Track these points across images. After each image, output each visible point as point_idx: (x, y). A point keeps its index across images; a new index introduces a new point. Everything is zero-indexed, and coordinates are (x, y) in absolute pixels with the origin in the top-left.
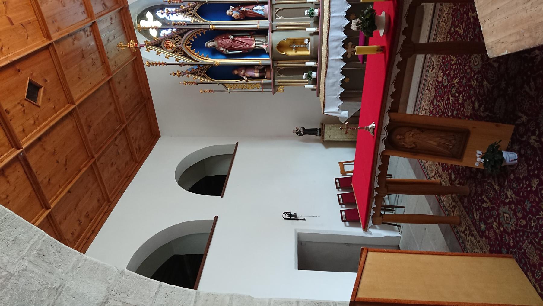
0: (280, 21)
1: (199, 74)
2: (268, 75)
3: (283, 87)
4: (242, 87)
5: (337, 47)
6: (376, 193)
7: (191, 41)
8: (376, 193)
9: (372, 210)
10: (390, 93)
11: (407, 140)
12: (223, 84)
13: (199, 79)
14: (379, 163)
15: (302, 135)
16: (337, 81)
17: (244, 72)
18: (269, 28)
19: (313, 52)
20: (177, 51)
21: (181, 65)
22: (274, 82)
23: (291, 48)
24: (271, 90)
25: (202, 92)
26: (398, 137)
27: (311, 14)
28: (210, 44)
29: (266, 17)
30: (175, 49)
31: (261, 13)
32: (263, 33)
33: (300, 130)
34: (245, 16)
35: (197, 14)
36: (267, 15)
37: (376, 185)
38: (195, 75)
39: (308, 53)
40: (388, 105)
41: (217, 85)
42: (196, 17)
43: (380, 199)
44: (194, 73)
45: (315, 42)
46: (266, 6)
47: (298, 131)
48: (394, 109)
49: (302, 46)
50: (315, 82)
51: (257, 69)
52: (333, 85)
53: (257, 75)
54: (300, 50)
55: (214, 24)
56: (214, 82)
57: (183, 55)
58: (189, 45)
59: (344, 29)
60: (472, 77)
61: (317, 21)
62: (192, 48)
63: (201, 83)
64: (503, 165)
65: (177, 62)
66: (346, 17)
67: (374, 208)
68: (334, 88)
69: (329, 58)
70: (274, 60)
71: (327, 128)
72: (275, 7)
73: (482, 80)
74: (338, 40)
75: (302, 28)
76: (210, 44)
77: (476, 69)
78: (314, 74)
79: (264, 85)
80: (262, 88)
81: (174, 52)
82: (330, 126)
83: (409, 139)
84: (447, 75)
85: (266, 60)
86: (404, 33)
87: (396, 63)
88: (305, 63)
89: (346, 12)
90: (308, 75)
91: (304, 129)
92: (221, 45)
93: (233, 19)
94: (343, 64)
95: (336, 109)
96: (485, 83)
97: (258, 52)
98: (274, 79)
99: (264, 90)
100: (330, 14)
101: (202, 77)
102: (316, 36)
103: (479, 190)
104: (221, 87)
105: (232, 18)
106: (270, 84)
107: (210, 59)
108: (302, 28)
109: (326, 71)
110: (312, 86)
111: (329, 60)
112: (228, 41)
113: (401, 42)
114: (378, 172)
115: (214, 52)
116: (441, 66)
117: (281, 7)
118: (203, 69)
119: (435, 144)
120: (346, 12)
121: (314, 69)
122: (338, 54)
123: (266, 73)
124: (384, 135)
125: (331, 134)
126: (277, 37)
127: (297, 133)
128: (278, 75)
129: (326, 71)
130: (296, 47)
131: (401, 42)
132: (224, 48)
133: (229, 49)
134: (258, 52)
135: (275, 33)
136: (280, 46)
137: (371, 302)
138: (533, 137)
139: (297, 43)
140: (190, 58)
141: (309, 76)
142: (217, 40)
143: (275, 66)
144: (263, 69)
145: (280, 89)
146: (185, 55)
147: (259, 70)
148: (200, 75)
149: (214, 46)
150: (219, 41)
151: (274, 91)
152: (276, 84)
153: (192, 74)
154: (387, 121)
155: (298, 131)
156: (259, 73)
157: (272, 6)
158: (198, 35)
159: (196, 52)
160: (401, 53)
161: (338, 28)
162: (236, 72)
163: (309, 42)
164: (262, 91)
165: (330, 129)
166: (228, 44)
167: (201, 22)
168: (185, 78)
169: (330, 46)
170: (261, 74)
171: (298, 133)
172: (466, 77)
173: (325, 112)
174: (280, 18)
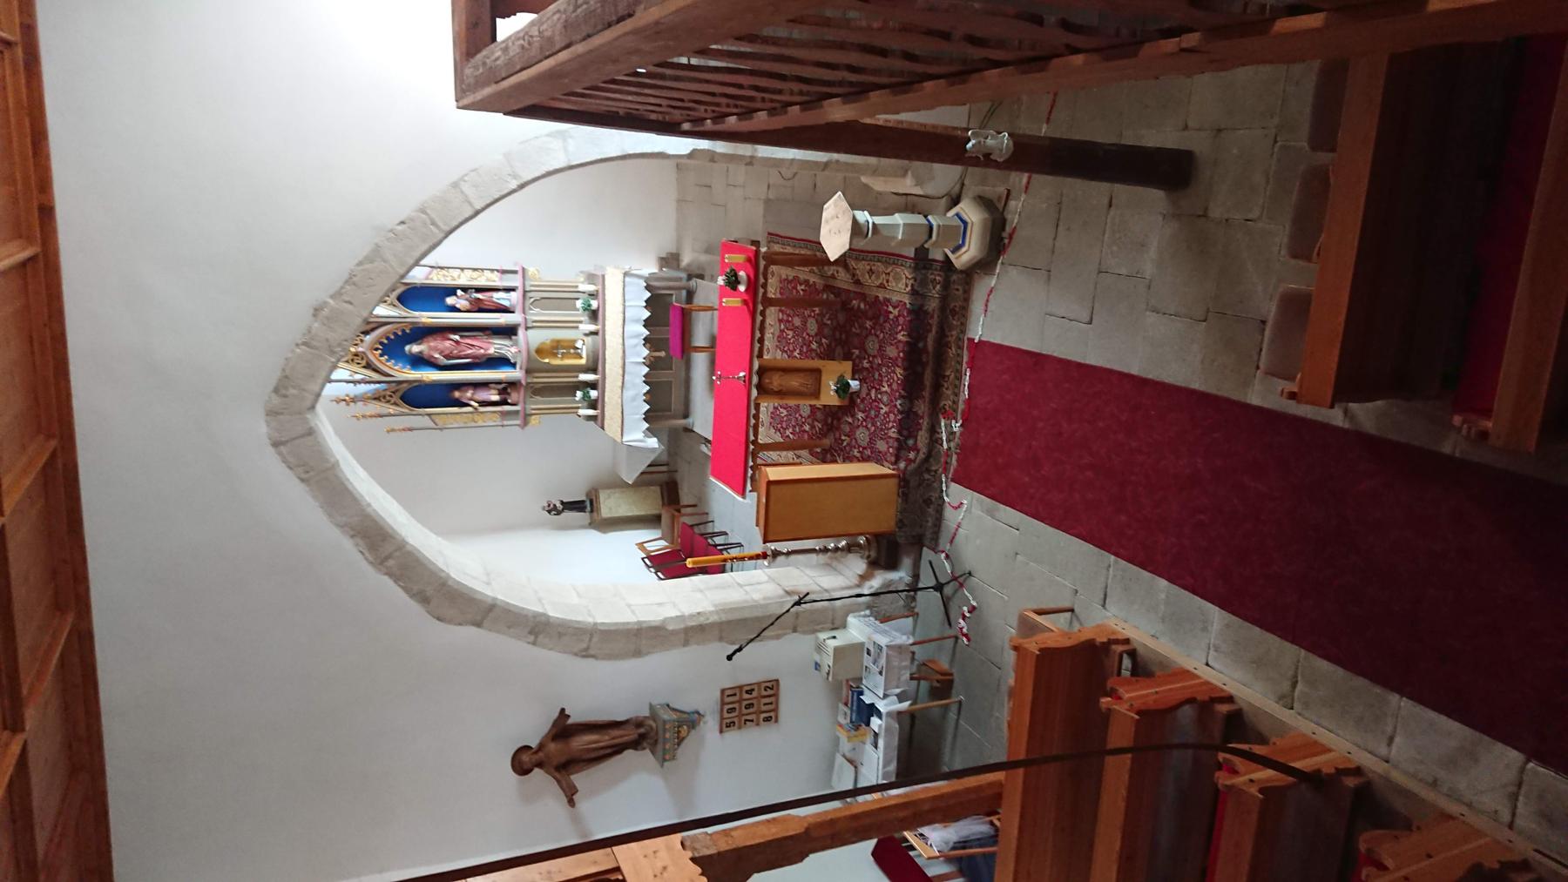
0: (536, 314)
1: (388, 398)
2: (513, 397)
3: (538, 416)
4: (466, 420)
5: (636, 346)
6: (752, 447)
7: (381, 343)
8: (752, 447)
9: (750, 470)
10: (757, 338)
11: (775, 384)
12: (429, 415)
13: (392, 409)
14: (753, 411)
15: (559, 513)
16: (637, 395)
17: (473, 394)
18: (519, 325)
19: (591, 360)
20: (352, 360)
21: (355, 382)
22: (525, 409)
23: (555, 355)
24: (518, 422)
25: (388, 432)
26: (767, 381)
27: (587, 308)
28: (415, 348)
29: (512, 310)
30: (350, 357)
31: (506, 303)
32: (509, 332)
33: (555, 505)
34: (479, 307)
35: (397, 303)
36: (514, 307)
37: (752, 438)
38: (380, 400)
39: (583, 361)
40: (756, 352)
41: (420, 418)
42: (394, 306)
43: (755, 456)
44: (377, 398)
45: (594, 344)
46: (512, 294)
47: (552, 506)
48: (760, 356)
49: (572, 351)
50: (593, 405)
51: (494, 389)
52: (634, 399)
53: (496, 398)
54: (568, 358)
55: (427, 317)
56: (414, 413)
57: (364, 367)
58: (377, 349)
59: (643, 323)
60: (811, 342)
61: (594, 315)
62: (381, 355)
63: (390, 415)
64: (851, 391)
65: (351, 378)
66: (645, 307)
67: (751, 467)
68: (635, 403)
69: (626, 361)
70: (528, 372)
71: (603, 496)
72: (529, 295)
73: (821, 339)
74: (637, 336)
75: (573, 325)
76: (415, 348)
77: (813, 333)
78: (594, 394)
79: (504, 414)
80: (503, 420)
81: (347, 362)
82: (608, 491)
83: (776, 381)
84: (786, 352)
85: (515, 374)
86: (762, 287)
87: (759, 311)
88: (577, 377)
89: (646, 301)
90: (584, 395)
91: (562, 503)
92: (436, 349)
93: (458, 310)
94: (646, 370)
95: (640, 436)
96: (824, 340)
97: (501, 361)
98: (525, 403)
99: (505, 423)
100: (624, 302)
101: (392, 404)
102: (595, 336)
103: (837, 436)
104: (426, 421)
105: (454, 309)
106: (517, 412)
107: (412, 372)
108: (573, 325)
109: (623, 379)
110: (591, 412)
111: (627, 364)
112: (448, 344)
113: (760, 295)
114: (753, 421)
115: (419, 361)
116: (777, 346)
117: (538, 295)
118: (397, 391)
119: (797, 384)
120: (646, 301)
121: (593, 386)
122: (638, 355)
123: (509, 394)
124: (755, 379)
125: (612, 505)
126: (537, 337)
127: (549, 512)
128: (532, 397)
129: (623, 379)
130: (563, 353)
131: (760, 295)
132: (440, 354)
133: (447, 357)
134: (501, 361)
135: (530, 331)
136: (539, 351)
137: (853, 67)
138: (866, 361)
139: (555, 348)
140: (376, 370)
141: (586, 396)
142: (429, 342)
143: (529, 381)
144: (507, 387)
145: (534, 420)
146: (369, 366)
147: (498, 390)
148: (388, 402)
149: (421, 352)
150: (432, 344)
151: (525, 423)
152: (528, 412)
153: (375, 399)
154: (756, 366)
155: (552, 506)
156: (499, 394)
157: (525, 292)
158: (395, 334)
159: (387, 361)
160: (762, 303)
161: (637, 321)
162: (457, 394)
163: (584, 344)
164: (502, 426)
165: (609, 497)
166: (447, 348)
167: (404, 314)
168: (359, 408)
169: (626, 344)
170: (503, 396)
171: (552, 510)
172: (805, 344)
173: (624, 440)
174: (537, 310)
